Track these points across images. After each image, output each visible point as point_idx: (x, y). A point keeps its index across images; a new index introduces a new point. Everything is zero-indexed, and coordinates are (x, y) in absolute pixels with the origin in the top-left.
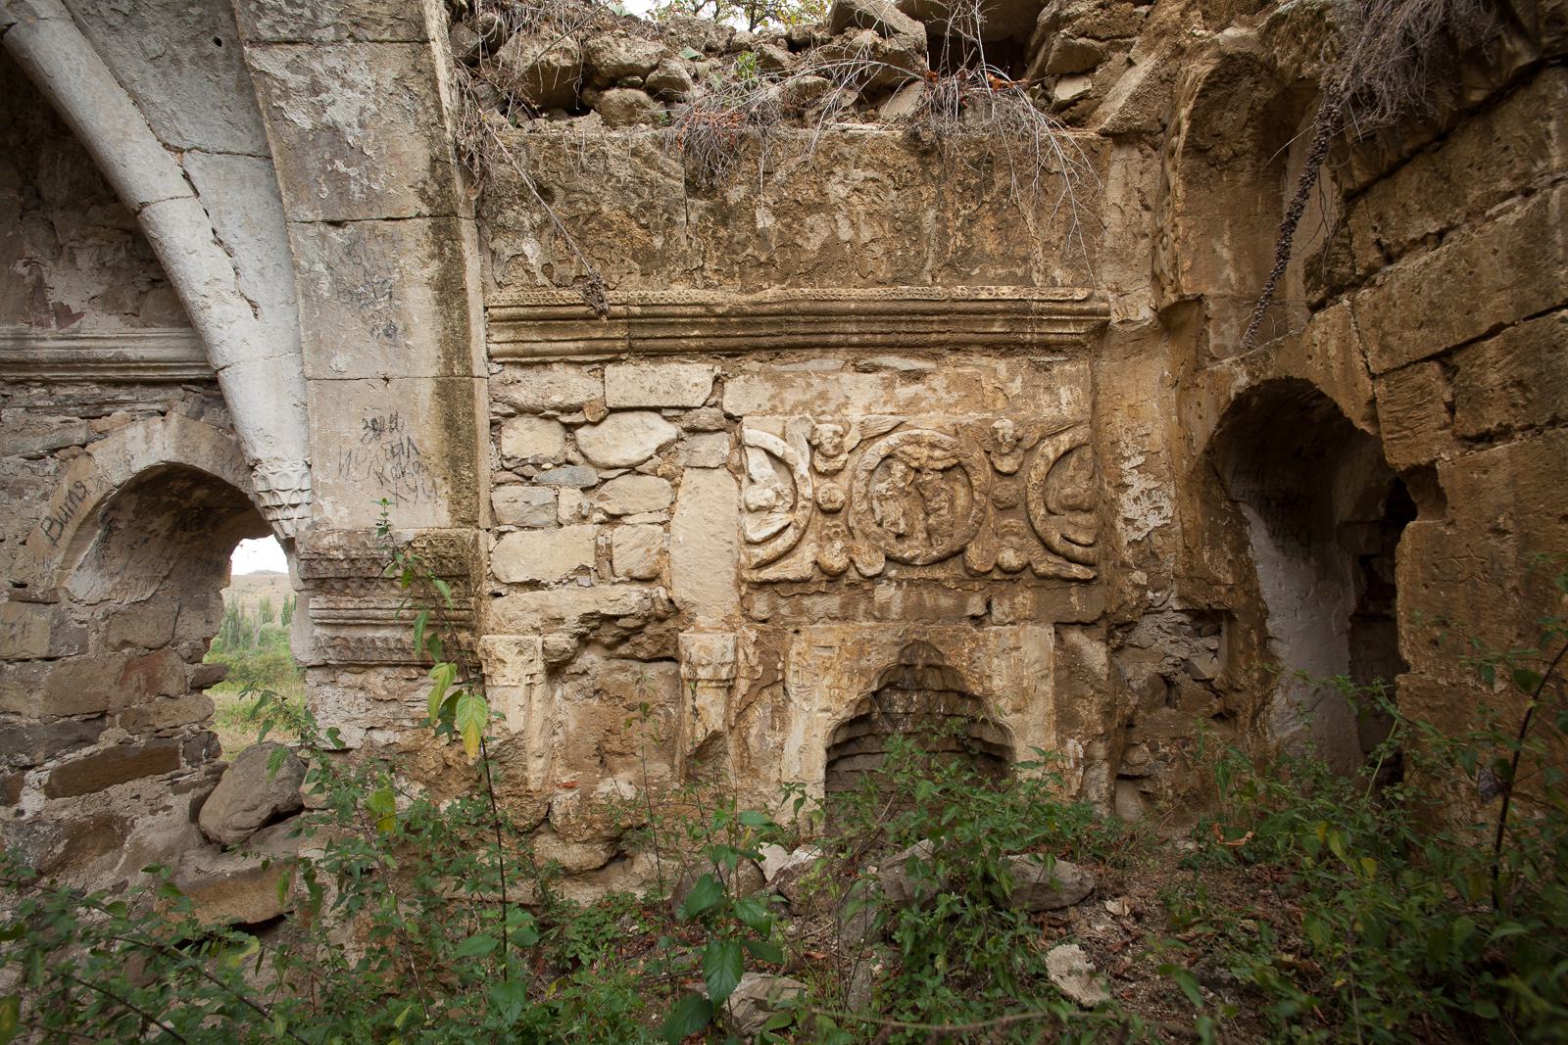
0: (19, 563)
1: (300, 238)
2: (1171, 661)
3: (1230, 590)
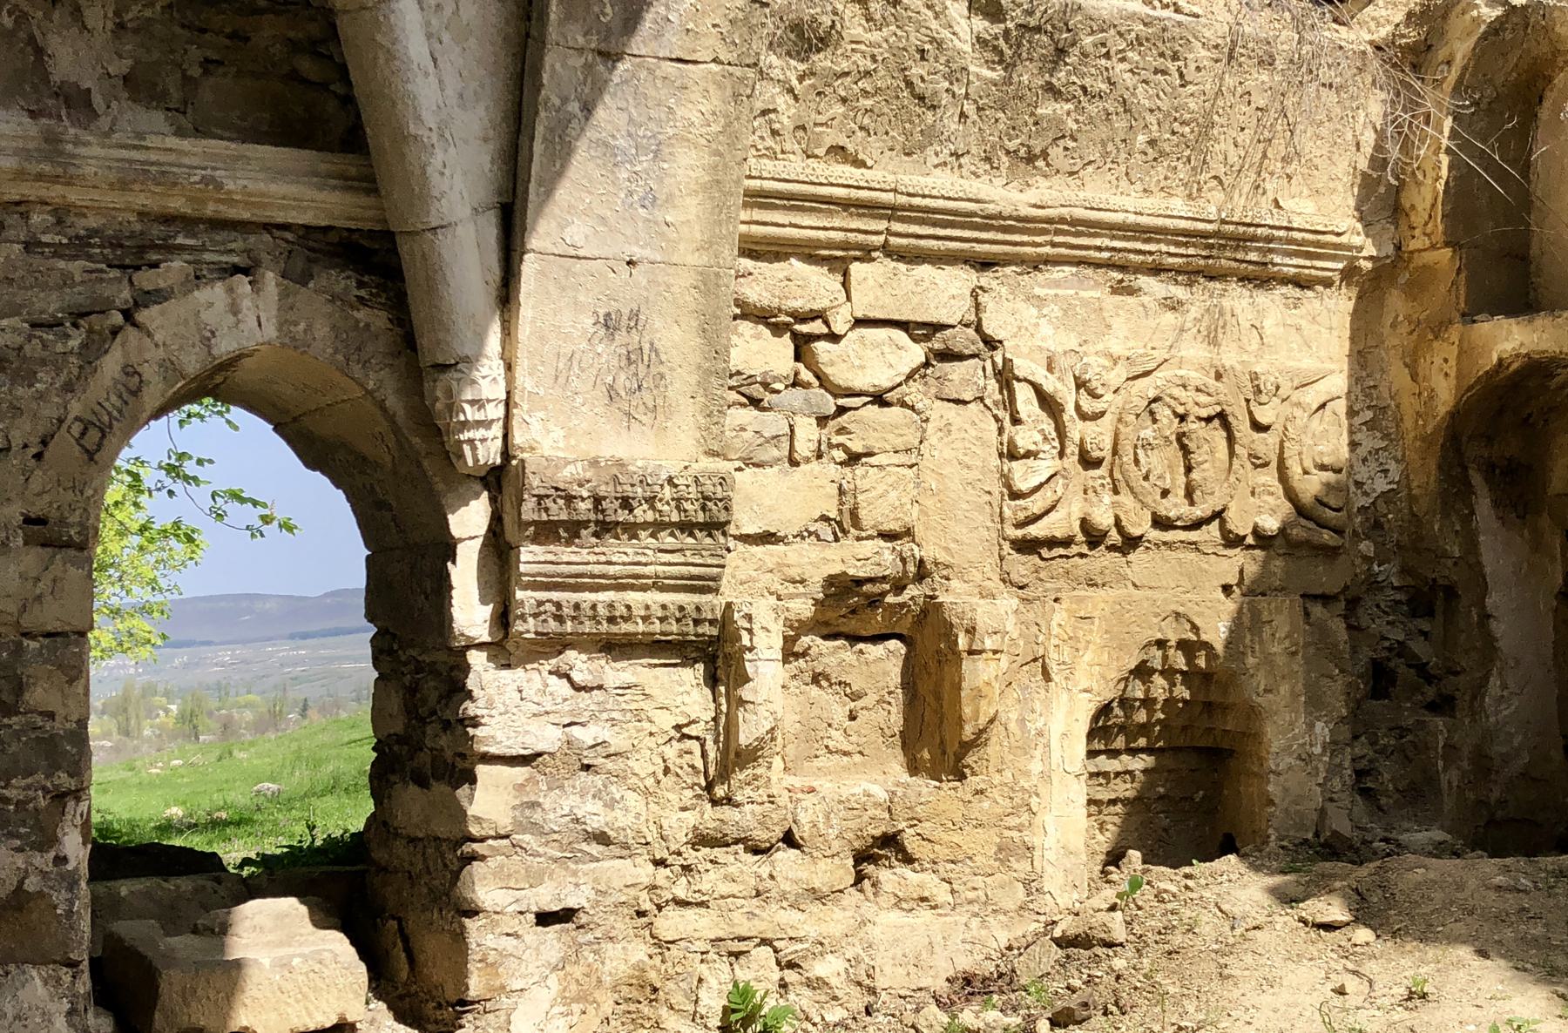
0: (35, 485)
1: (558, 66)
2: (1387, 644)
3: (1455, 564)
